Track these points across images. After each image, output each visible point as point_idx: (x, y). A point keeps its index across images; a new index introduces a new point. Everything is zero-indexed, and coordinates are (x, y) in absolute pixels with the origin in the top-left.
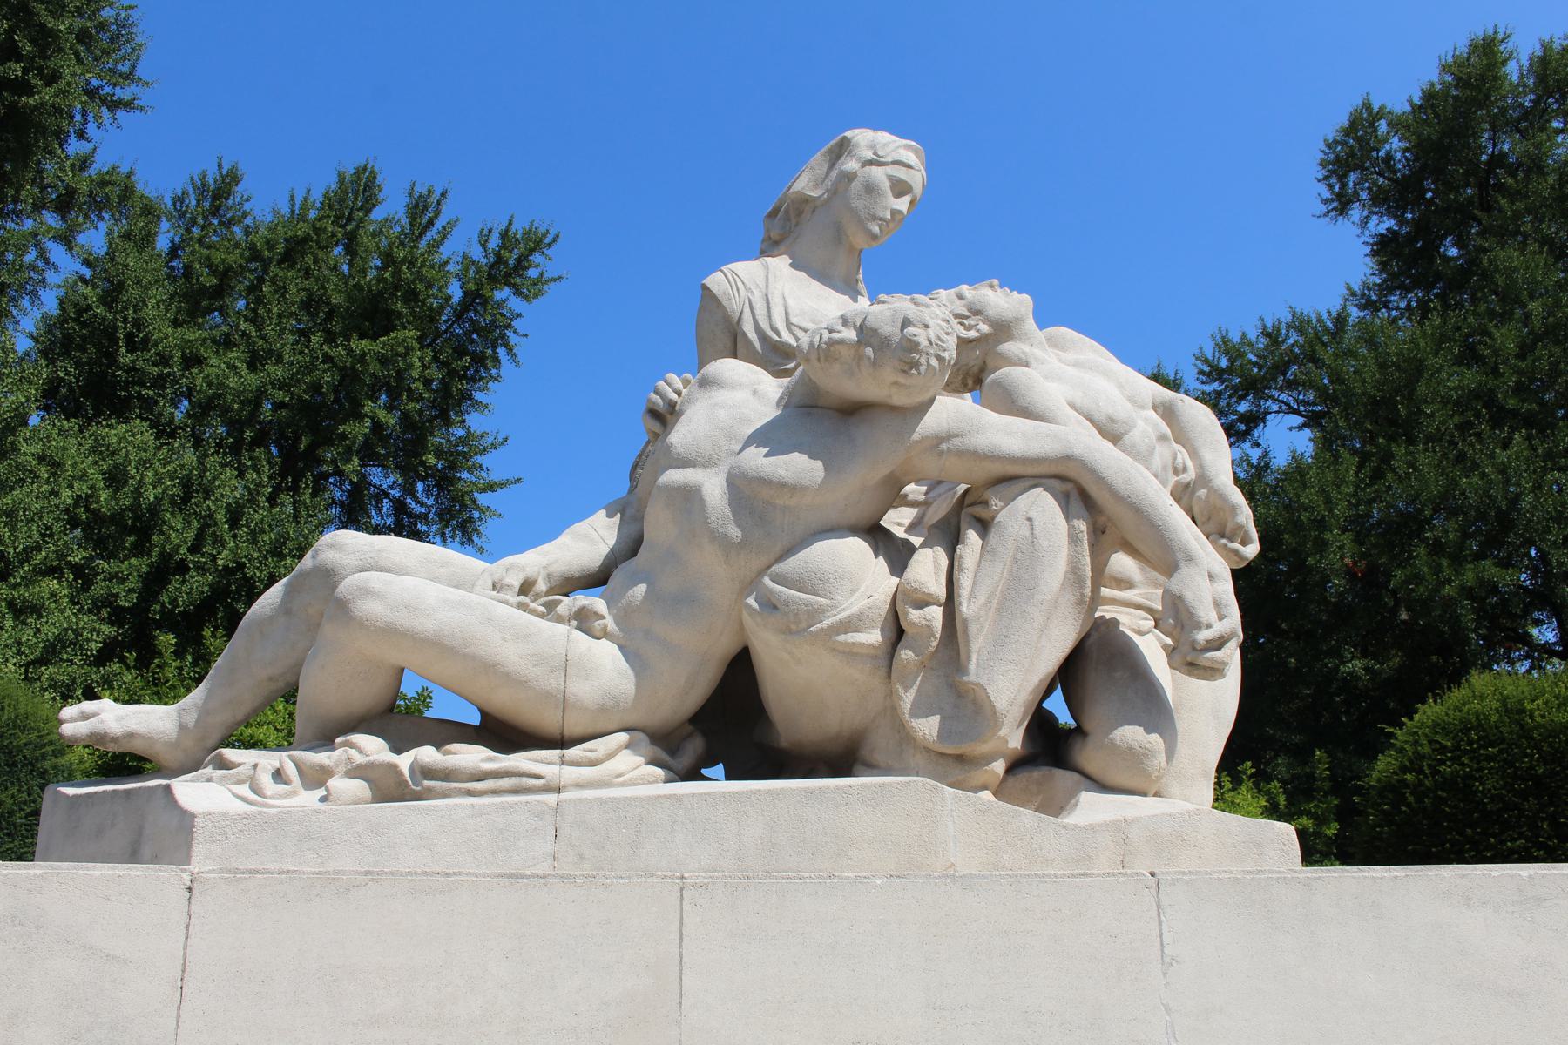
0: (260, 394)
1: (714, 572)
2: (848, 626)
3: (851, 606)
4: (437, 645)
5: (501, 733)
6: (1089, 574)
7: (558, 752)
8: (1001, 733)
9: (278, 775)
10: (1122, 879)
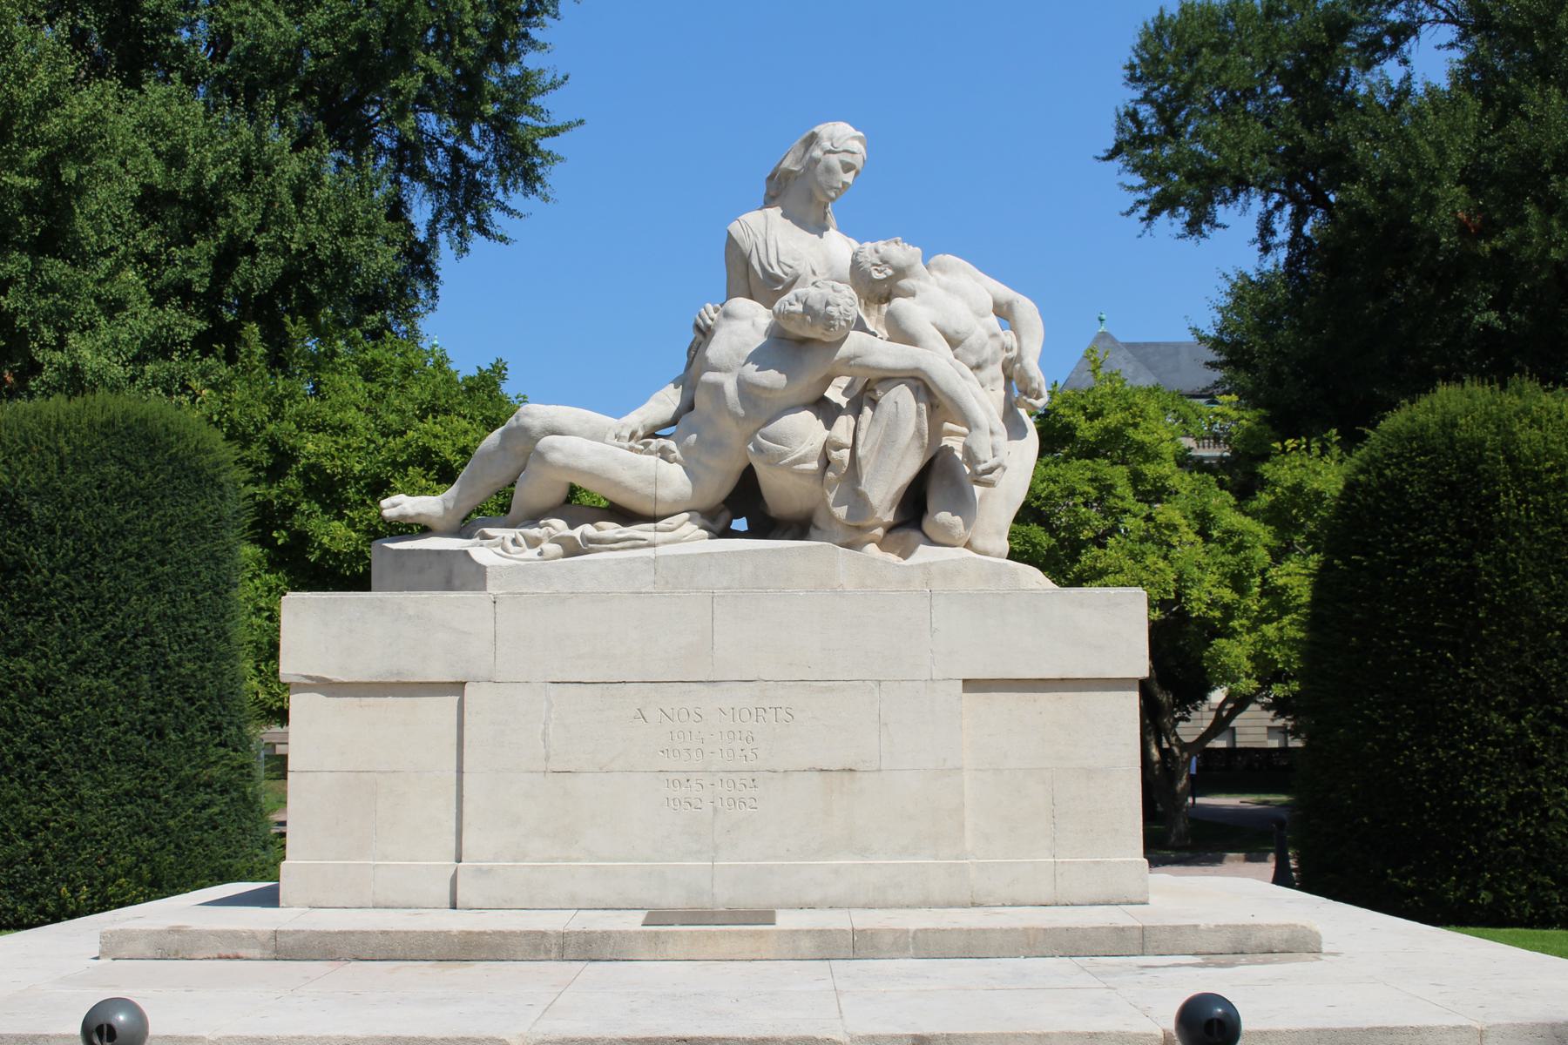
0: (302, 44)
3: (801, 451)
4: (590, 474)
5: (625, 515)
7: (651, 526)
9: (514, 541)
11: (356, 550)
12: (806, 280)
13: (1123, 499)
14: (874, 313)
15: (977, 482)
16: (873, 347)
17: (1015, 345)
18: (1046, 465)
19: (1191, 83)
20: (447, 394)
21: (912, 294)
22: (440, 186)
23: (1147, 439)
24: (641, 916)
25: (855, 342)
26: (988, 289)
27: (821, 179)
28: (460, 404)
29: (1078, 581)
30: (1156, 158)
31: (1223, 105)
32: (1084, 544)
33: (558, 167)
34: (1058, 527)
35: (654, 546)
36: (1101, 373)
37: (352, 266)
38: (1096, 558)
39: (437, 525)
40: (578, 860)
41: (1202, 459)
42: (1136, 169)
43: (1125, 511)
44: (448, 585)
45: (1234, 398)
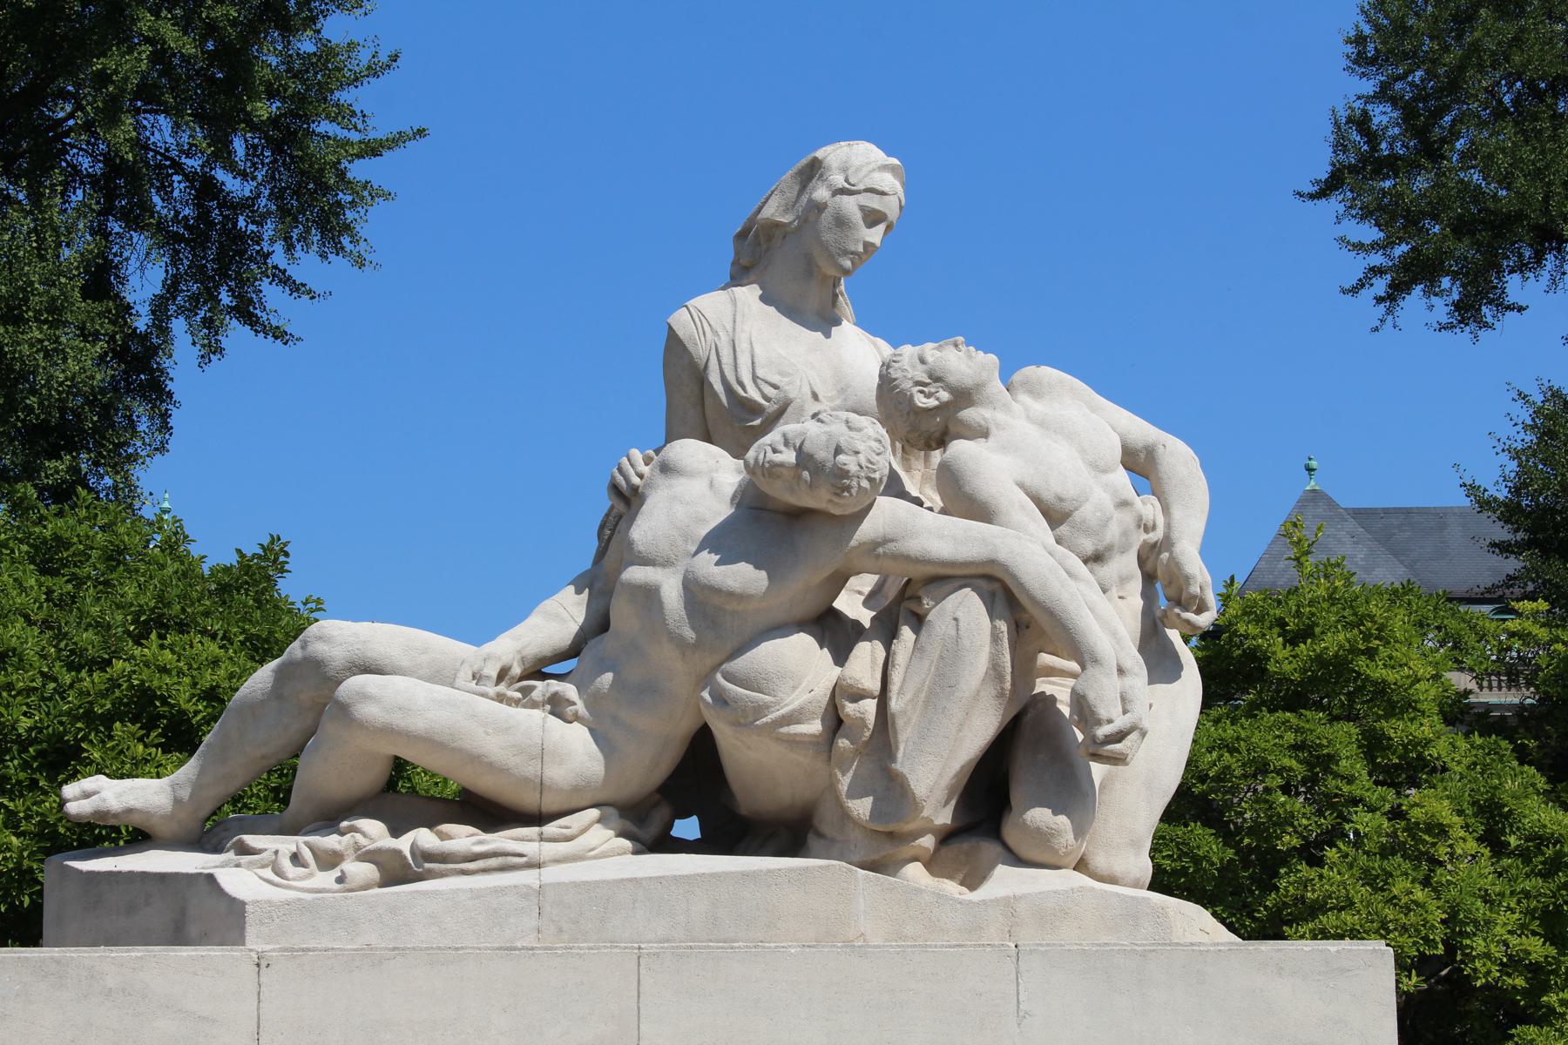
1: (676, 669)
2: (789, 719)
3: (793, 701)
4: (429, 741)
5: (489, 813)
6: (1009, 670)
7: (535, 830)
8: (925, 813)
11: (19, 864)
12: (801, 409)
13: (1350, 780)
14: (918, 464)
15: (1097, 757)
16: (923, 528)
17: (1160, 521)
18: (1217, 721)
19: (1461, 68)
20: (184, 596)
21: (984, 434)
22: (178, 238)
23: (1391, 676)
25: (885, 515)
26: (1111, 424)
27: (828, 237)
28: (207, 614)
29: (1271, 929)
30: (1400, 195)
31: (1516, 102)
32: (1283, 859)
33: (378, 209)
34: (1239, 829)
35: (539, 866)
36: (1309, 563)
37: (23, 376)
38: (1305, 883)
39: (163, 829)
41: (1489, 707)
42: (1365, 214)
43: (1355, 801)
44: (178, 936)
45: (1542, 605)
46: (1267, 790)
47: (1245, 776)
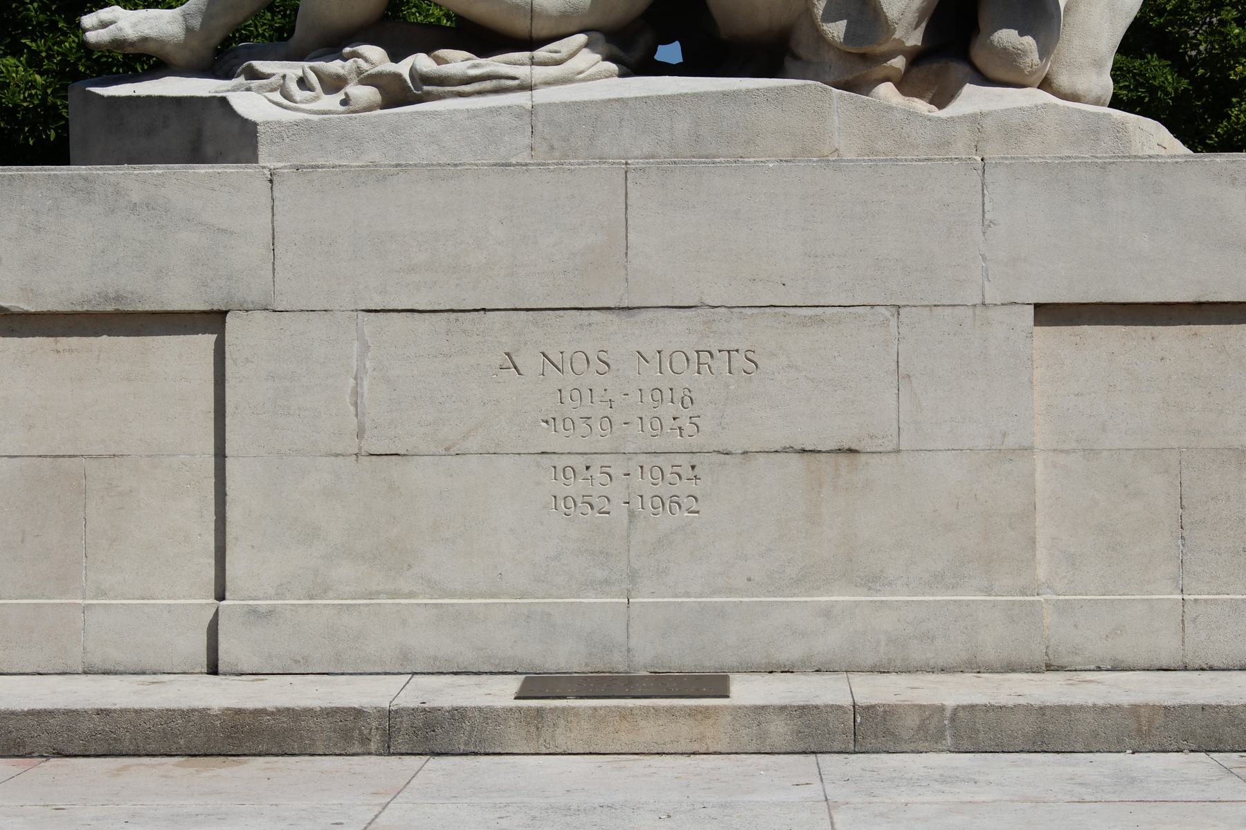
7: (527, 54)
8: (897, 36)
10: (956, 163)
24: (513, 684)
40: (411, 595)
44: (195, 155)
46: (1223, 23)
47: (1201, 10)
